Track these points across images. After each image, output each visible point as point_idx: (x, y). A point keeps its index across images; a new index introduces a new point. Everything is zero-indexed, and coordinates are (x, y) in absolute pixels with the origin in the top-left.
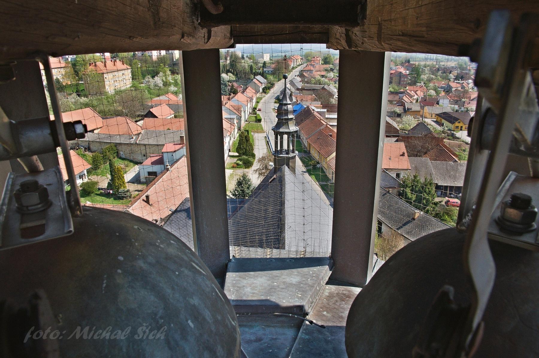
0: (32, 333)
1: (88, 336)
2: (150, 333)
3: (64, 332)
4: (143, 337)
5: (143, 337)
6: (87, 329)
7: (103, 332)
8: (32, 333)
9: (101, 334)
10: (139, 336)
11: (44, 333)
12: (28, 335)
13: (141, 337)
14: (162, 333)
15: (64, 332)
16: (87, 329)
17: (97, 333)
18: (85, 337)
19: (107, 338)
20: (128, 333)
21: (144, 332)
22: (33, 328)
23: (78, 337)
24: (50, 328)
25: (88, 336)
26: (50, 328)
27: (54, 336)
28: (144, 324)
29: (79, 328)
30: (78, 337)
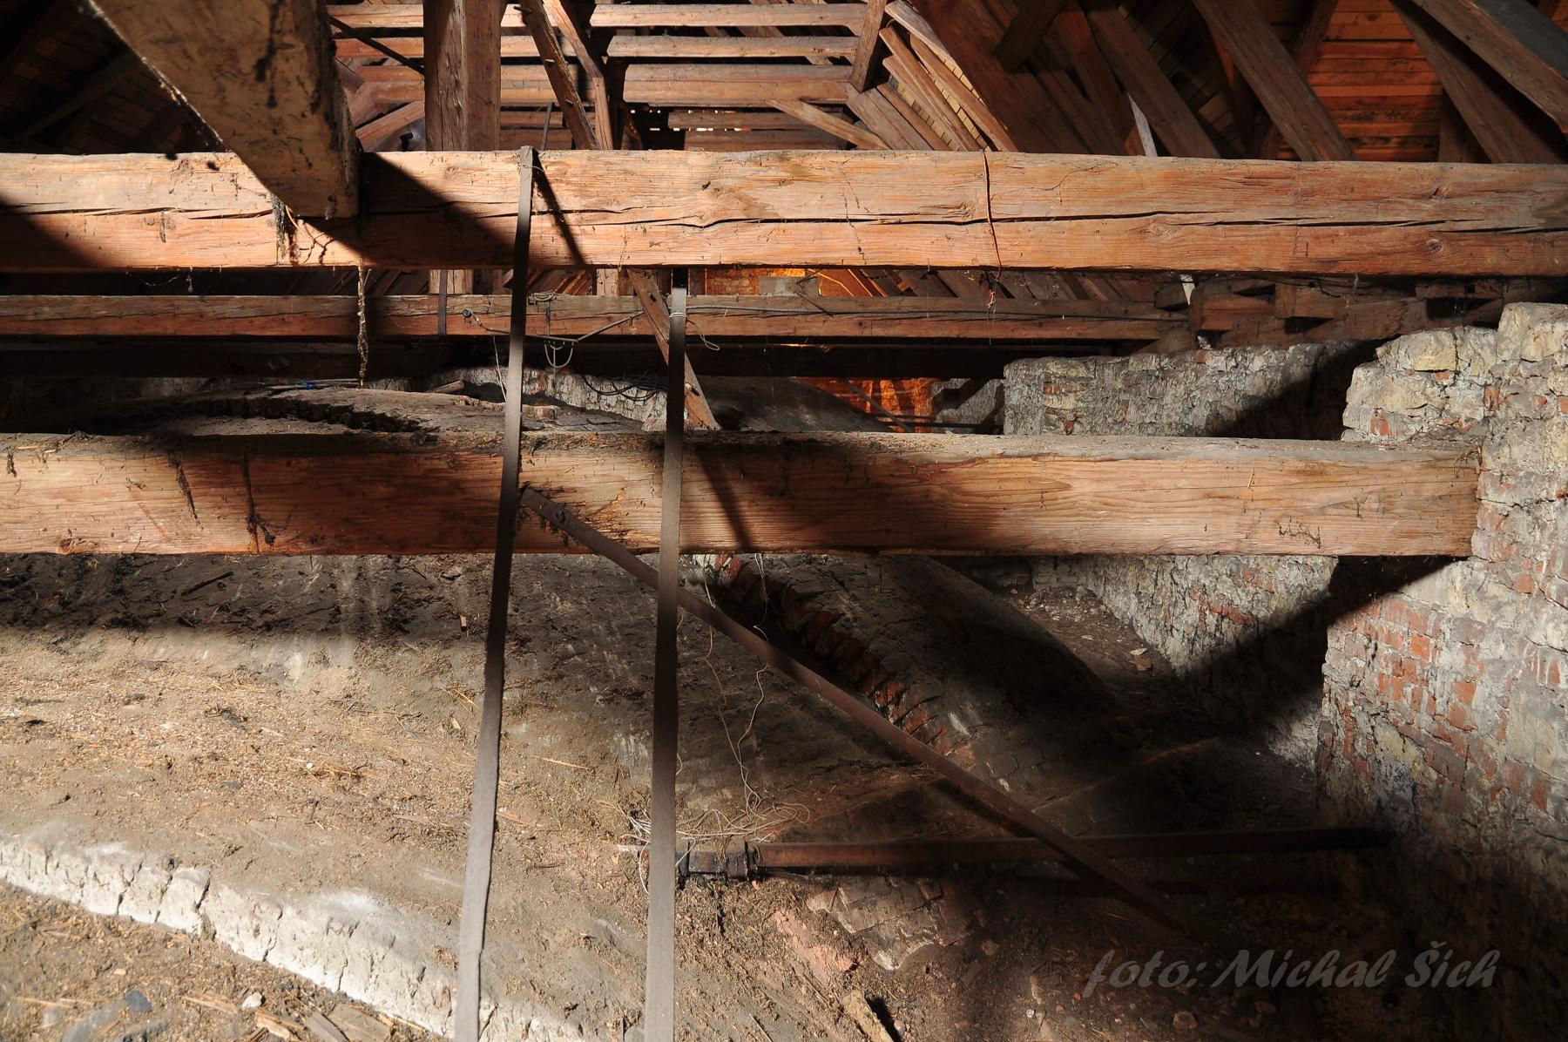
0: (1107, 973)
1: (1270, 978)
2: (1288, 972)
3: (1201, 966)
4: (1429, 981)
5: (1429, 981)
6: (1268, 955)
7: (1473, 967)
8: (1107, 973)
9: (1468, 973)
10: (1417, 978)
11: (1142, 968)
13: (1423, 981)
14: (1486, 968)
15: (1201, 966)
16: (1268, 955)
17: (1296, 971)
18: (1262, 980)
19: (1326, 983)
20: (1385, 968)
21: (1433, 968)
24: (1160, 954)
25: (1270, 978)
26: (1160, 954)
27: (1174, 975)
28: (1435, 944)
29: (1244, 955)
30: (1241, 979)
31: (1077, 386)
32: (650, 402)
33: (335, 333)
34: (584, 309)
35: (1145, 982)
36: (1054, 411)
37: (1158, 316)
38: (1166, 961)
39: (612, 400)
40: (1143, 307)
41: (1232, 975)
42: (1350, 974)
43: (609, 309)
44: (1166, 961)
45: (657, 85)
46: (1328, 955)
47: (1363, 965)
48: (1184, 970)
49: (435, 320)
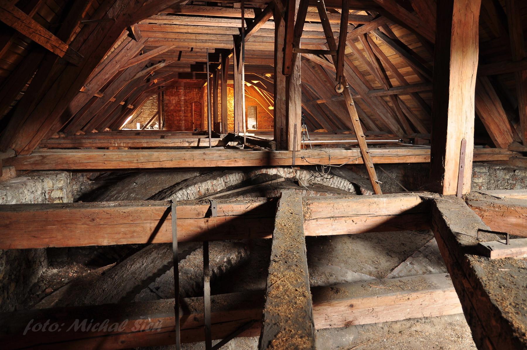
0: (31, 326)
1: (86, 328)
3: (63, 325)
6: (85, 321)
7: (100, 325)
8: (31, 326)
12: (28, 328)
14: (104, 325)
15: (63, 325)
16: (85, 321)
17: (95, 326)
18: (83, 329)
19: (105, 330)
22: (32, 320)
23: (76, 329)
24: (49, 321)
25: (86, 328)
26: (49, 321)
27: (54, 328)
28: (522, 340)
29: (77, 321)
30: (76, 329)
31: (483, 175)
32: (332, 179)
33: (258, 165)
34: (341, 155)
35: (44, 330)
36: (476, 183)
37: (508, 153)
38: (51, 323)
39: (319, 179)
40: (505, 150)
41: (74, 327)
42: (113, 327)
43: (349, 155)
44: (51, 323)
45: (257, 44)
46: (106, 321)
47: (117, 324)
48: (57, 326)
49: (291, 160)
